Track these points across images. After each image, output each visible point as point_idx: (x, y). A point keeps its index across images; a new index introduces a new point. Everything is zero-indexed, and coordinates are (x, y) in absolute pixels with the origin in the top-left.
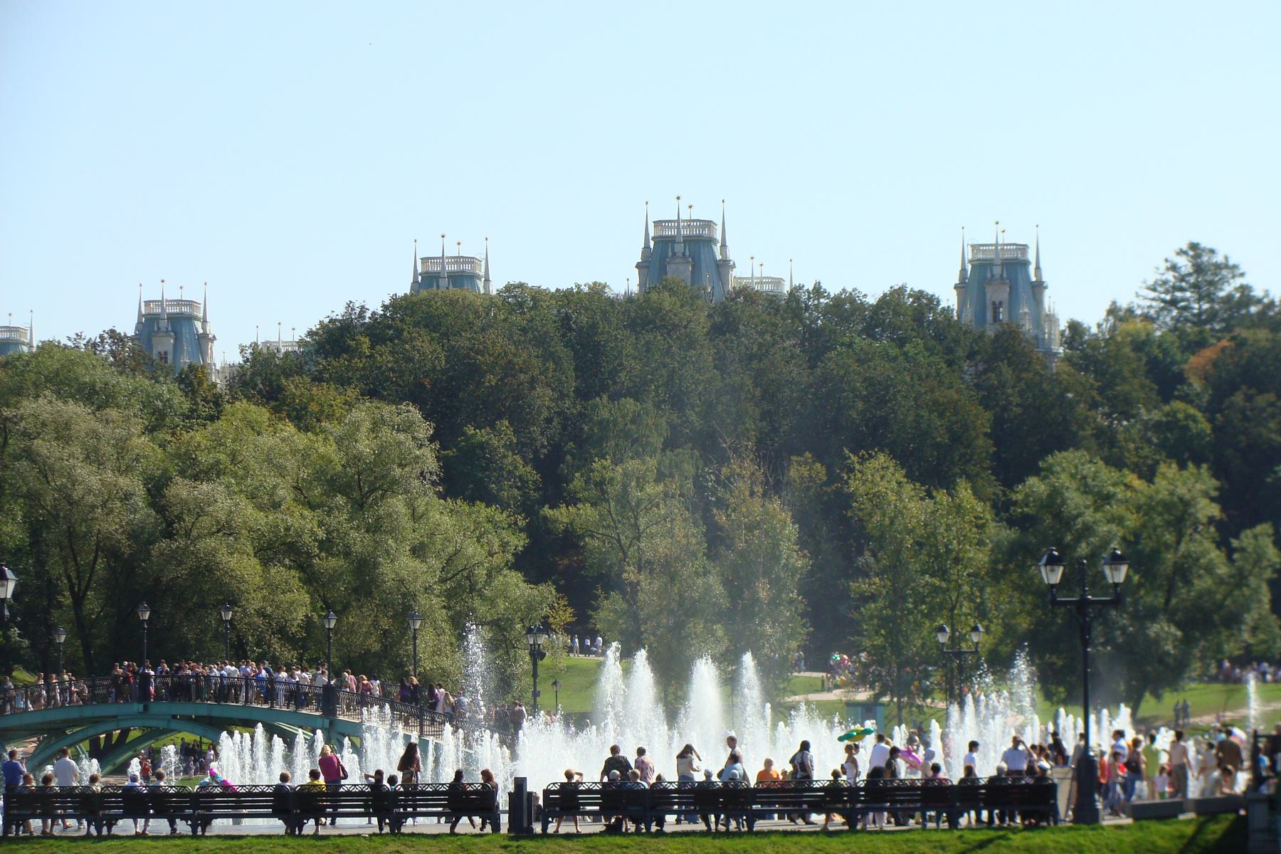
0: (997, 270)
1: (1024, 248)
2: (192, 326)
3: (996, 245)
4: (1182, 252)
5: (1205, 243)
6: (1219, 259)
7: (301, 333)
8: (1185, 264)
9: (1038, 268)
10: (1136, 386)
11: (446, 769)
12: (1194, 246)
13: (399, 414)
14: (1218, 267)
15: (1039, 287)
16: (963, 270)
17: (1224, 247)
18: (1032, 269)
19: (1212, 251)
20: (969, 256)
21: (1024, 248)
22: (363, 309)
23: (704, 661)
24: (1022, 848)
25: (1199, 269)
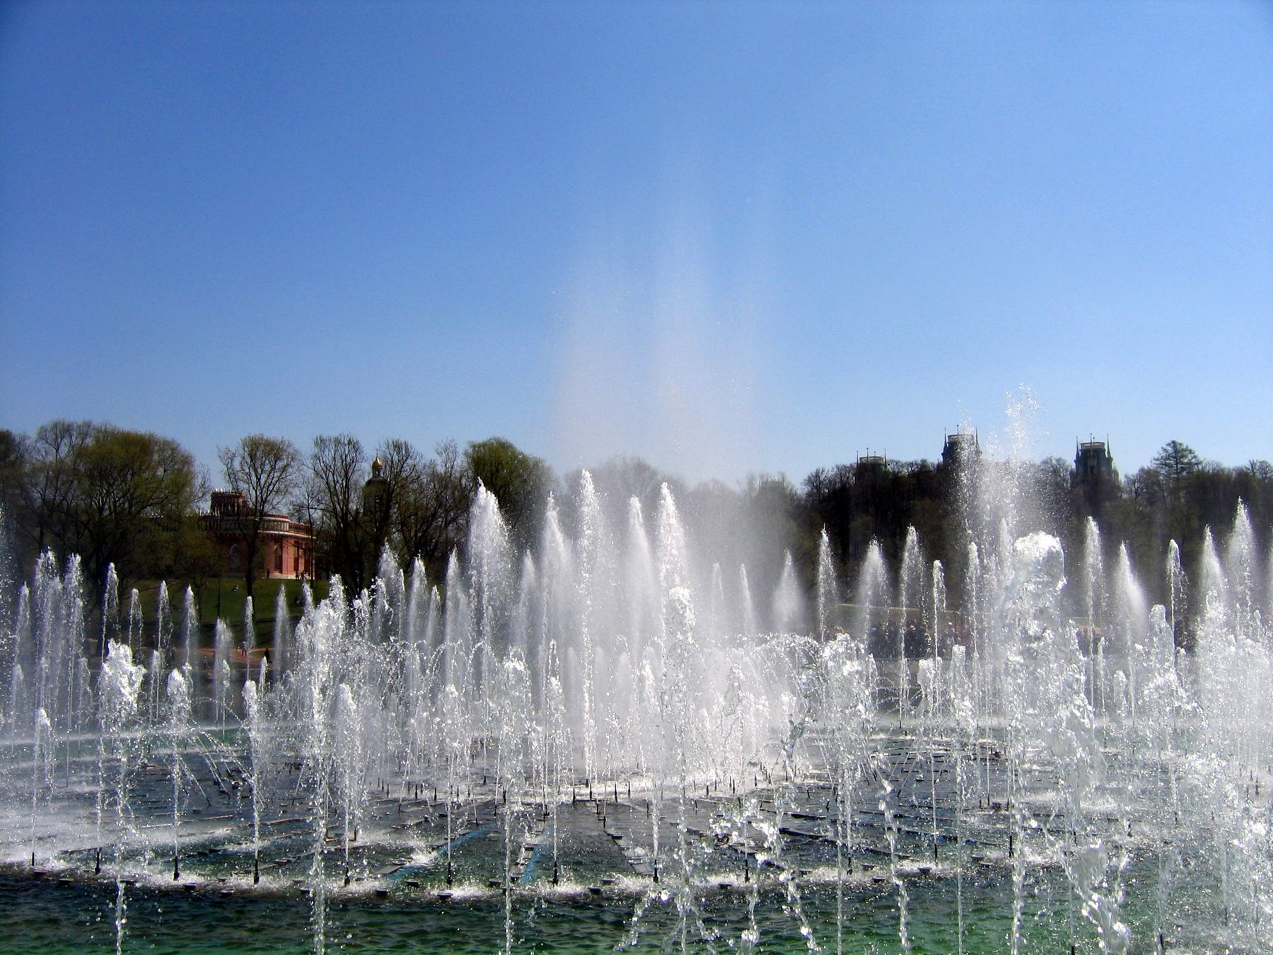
0: (1092, 453)
1: (1103, 444)
2: (880, 469)
3: (1091, 443)
4: (1169, 445)
5: (1179, 441)
6: (1184, 447)
7: (1232, 466)
8: (1170, 449)
9: (1109, 452)
11: (190, 610)
12: (1174, 442)
13: (948, 744)
14: (1183, 450)
15: (1110, 459)
16: (1078, 454)
17: (1185, 441)
18: (1106, 452)
19: (1181, 444)
20: (1080, 448)
21: (1103, 444)
23: (423, 461)
24: (201, 700)
25: (1176, 451)
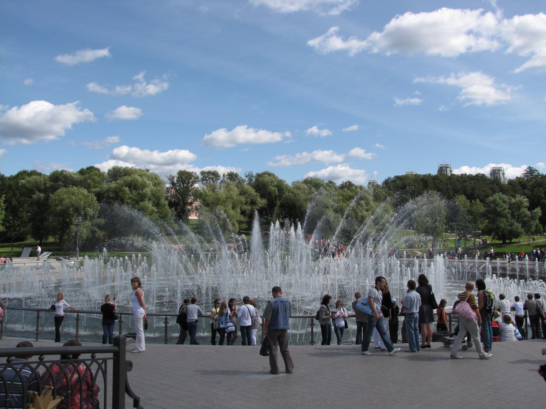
4: (528, 168)
6: (534, 169)
10: (519, 188)
12: (530, 167)
14: (534, 170)
22: (391, 178)
25: (531, 171)
